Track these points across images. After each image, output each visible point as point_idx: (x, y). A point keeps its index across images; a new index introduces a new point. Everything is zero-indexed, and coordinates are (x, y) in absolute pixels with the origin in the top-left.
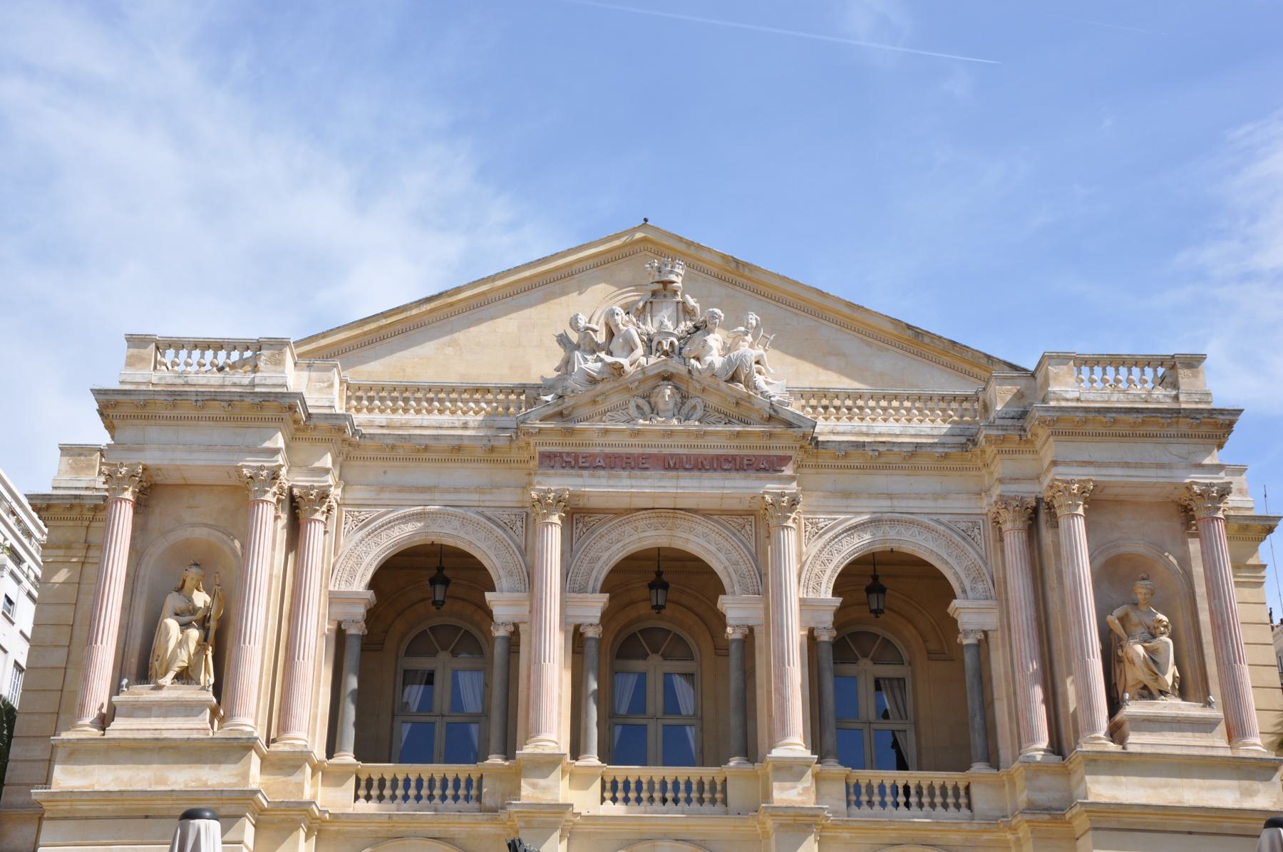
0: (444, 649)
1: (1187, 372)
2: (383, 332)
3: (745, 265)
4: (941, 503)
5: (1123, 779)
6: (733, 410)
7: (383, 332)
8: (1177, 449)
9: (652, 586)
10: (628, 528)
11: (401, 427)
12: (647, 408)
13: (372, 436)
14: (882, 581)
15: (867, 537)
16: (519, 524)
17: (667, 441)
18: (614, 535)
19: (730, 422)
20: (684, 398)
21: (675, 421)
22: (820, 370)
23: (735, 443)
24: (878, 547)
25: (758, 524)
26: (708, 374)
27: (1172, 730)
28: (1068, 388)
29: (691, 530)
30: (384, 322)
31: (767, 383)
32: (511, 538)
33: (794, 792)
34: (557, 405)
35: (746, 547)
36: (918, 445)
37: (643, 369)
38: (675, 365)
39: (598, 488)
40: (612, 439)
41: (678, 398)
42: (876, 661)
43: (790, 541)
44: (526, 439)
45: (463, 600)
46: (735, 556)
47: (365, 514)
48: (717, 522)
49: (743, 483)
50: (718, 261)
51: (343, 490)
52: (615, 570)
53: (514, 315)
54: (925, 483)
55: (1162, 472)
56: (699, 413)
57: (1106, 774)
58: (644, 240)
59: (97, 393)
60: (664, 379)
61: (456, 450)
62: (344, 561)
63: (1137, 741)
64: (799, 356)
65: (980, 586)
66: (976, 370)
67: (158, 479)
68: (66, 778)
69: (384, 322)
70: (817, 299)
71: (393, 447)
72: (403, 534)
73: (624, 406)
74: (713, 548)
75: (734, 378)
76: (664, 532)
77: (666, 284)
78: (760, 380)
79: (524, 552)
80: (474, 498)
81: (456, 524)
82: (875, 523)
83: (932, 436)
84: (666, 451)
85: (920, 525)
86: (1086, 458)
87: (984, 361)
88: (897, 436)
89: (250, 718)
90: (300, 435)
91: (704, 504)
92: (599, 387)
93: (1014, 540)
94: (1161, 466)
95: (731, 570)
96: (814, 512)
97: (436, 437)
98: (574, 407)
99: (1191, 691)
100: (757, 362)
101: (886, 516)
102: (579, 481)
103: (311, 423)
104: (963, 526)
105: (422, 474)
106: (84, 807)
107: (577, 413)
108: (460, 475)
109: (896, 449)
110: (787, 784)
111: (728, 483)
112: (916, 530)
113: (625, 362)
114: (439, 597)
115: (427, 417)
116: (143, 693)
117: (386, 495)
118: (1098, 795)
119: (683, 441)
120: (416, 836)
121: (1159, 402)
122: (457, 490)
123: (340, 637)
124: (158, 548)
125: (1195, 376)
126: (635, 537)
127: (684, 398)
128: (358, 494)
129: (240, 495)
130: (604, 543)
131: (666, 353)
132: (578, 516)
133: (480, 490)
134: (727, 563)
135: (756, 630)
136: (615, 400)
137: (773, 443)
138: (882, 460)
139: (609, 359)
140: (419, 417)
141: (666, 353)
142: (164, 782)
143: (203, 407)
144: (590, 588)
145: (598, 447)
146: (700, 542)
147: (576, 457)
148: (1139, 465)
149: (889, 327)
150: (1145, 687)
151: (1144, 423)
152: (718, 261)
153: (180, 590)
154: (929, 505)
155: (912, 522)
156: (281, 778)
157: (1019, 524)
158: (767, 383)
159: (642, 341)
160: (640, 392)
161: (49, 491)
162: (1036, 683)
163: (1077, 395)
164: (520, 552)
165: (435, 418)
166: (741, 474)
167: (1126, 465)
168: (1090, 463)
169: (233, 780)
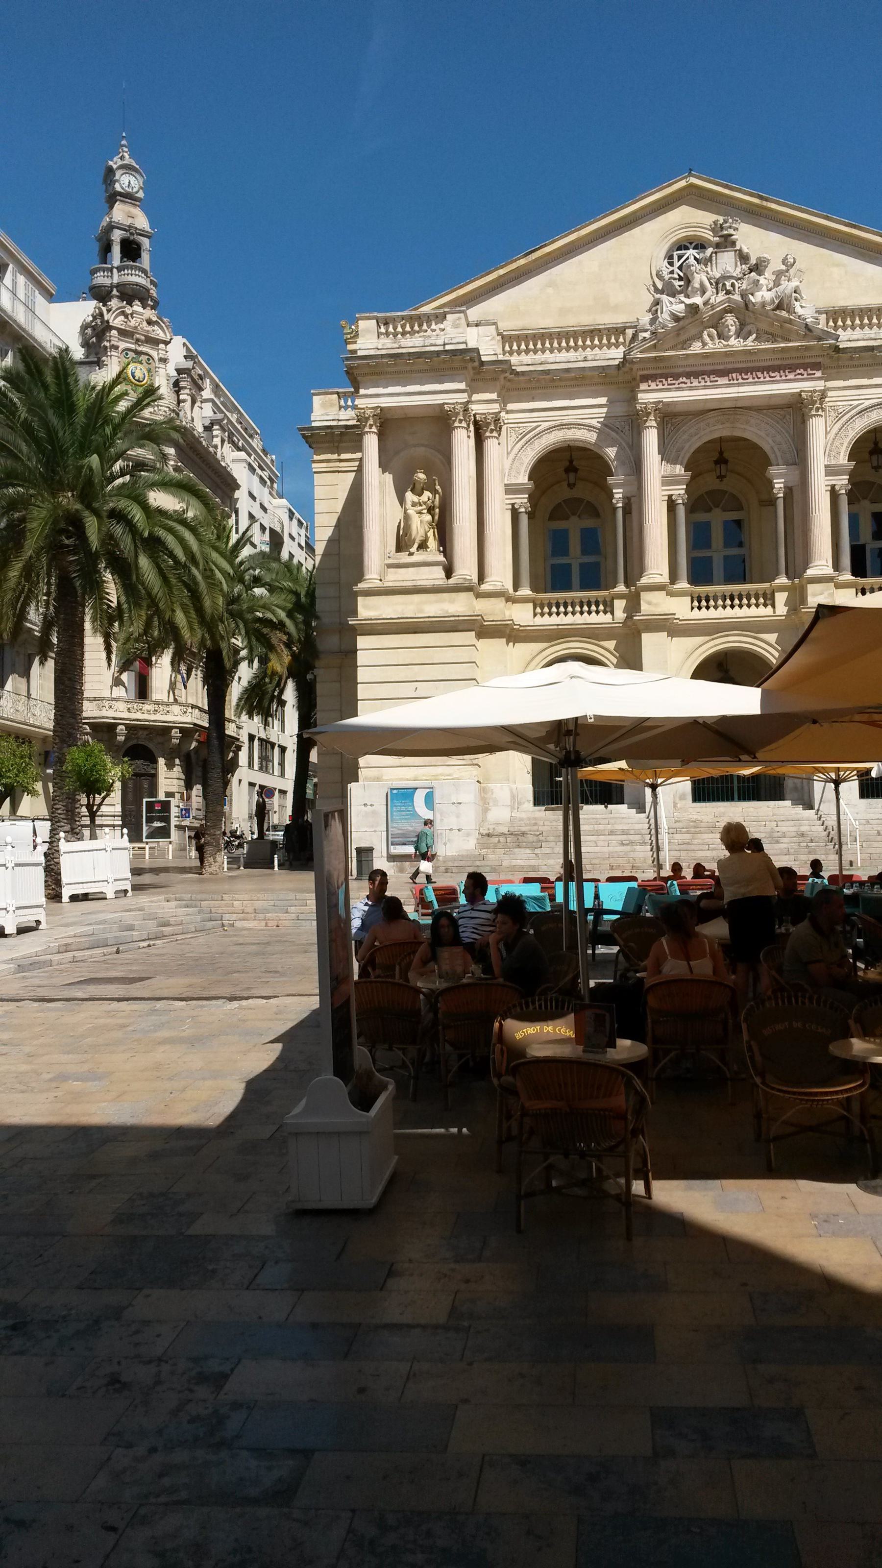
13: (523, 373)
14: (726, 455)
16: (627, 428)
18: (692, 430)
19: (776, 341)
25: (796, 413)
29: (747, 422)
31: (802, 307)
32: (622, 438)
35: (787, 432)
44: (630, 366)
45: (739, 474)
46: (779, 438)
48: (766, 415)
62: (510, 463)
67: (389, 416)
74: (762, 434)
75: (779, 307)
78: (798, 309)
79: (631, 447)
89: (466, 569)
92: (681, 323)
95: (776, 449)
97: (568, 370)
100: (795, 292)
114: (572, 481)
115: (558, 355)
116: (404, 557)
118: (540, 811)
130: (685, 437)
134: (773, 444)
135: (794, 489)
139: (688, 301)
140: (553, 355)
142: (421, 611)
146: (753, 431)
158: (802, 307)
159: (711, 284)
164: (629, 447)
165: (564, 356)
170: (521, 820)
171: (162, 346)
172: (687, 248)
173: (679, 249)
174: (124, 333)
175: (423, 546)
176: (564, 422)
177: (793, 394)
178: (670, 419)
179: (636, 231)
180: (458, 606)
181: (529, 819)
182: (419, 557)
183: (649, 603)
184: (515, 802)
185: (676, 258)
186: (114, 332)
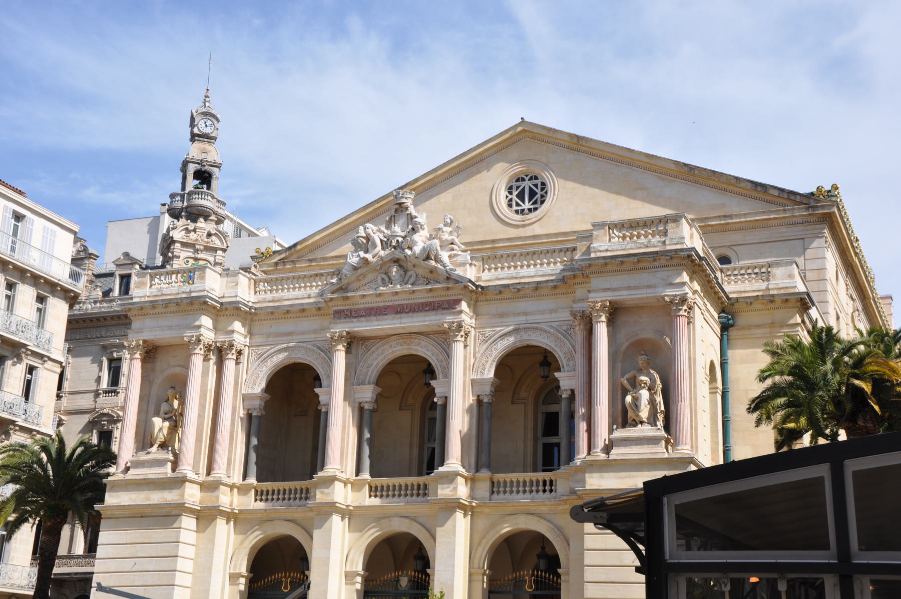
1: (673, 225)
2: (378, 212)
3: (583, 138)
4: (554, 315)
5: (606, 474)
6: (430, 276)
7: (378, 212)
8: (662, 274)
10: (387, 346)
11: (279, 301)
12: (387, 279)
13: (261, 308)
15: (512, 339)
17: (395, 298)
18: (380, 351)
20: (406, 271)
21: (398, 286)
22: (631, 201)
23: (430, 294)
24: (519, 345)
25: (444, 338)
26: (412, 258)
27: (637, 444)
28: (606, 245)
29: (419, 344)
30: (377, 206)
33: (448, 490)
34: (337, 284)
36: (538, 282)
37: (382, 258)
38: (398, 254)
39: (362, 327)
40: (367, 299)
41: (402, 273)
43: (458, 349)
47: (261, 350)
49: (434, 318)
50: (566, 138)
51: (250, 339)
53: (450, 191)
54: (547, 304)
55: (650, 291)
56: (411, 281)
57: (597, 472)
58: (524, 131)
60: (395, 262)
61: (303, 310)
62: (248, 379)
64: (618, 193)
66: (731, 188)
67: (157, 344)
68: (111, 499)
69: (377, 206)
70: (627, 154)
71: (272, 313)
72: (279, 359)
73: (375, 280)
75: (428, 258)
76: (405, 347)
77: (400, 204)
80: (312, 337)
81: (303, 351)
82: (516, 331)
83: (552, 275)
84: (396, 303)
85: (541, 329)
86: (609, 287)
87: (734, 181)
88: (533, 277)
90: (220, 313)
91: (423, 330)
92: (359, 271)
94: (649, 287)
96: (484, 328)
97: (291, 306)
98: (349, 284)
101: (522, 326)
102: (352, 325)
103: (224, 307)
104: (565, 328)
105: (288, 326)
106: (117, 513)
107: (351, 287)
108: (307, 324)
109: (526, 286)
110: (446, 486)
111: (426, 318)
112: (538, 333)
113: (369, 256)
116: (142, 456)
117: (271, 339)
119: (404, 296)
120: (279, 519)
121: (655, 246)
122: (304, 333)
123: (250, 416)
124: (159, 379)
125: (678, 227)
126: (391, 351)
127: (406, 271)
128: (258, 340)
129: (186, 349)
130: (374, 356)
131: (395, 247)
132: (353, 342)
133: (315, 332)
136: (370, 277)
137: (450, 292)
138: (521, 293)
141: (395, 247)
142: (149, 499)
143: (166, 307)
144: (367, 382)
145: (362, 305)
146: (424, 350)
148: (636, 288)
149: (672, 167)
151: (639, 261)
152: (566, 138)
153: (167, 401)
154: (547, 317)
155: (536, 328)
156: (209, 494)
157: (582, 327)
160: (383, 271)
162: (583, 420)
163: (606, 247)
166: (435, 312)
167: (629, 288)
168: (609, 289)
169: (177, 498)
171: (220, 252)
172: (523, 180)
173: (518, 180)
174: (184, 245)
176: (788, 285)
185: (514, 188)
186: (178, 245)
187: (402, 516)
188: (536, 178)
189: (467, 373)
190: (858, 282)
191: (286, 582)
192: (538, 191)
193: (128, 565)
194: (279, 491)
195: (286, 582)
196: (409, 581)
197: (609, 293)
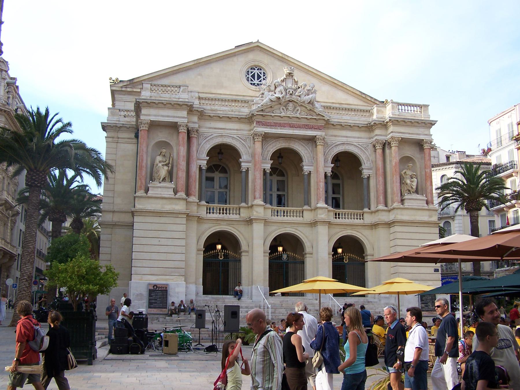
0: (217, 171)
9: (219, 153)
14: (223, 151)
42: (278, 175)
52: (274, 154)
55: (418, 136)
59: (102, 123)
63: (407, 204)
65: (369, 162)
93: (379, 151)
99: (419, 193)
104: (365, 146)
147: (266, 123)
150: (409, 191)
161: (106, 121)
170: (200, 300)
171: (4, 72)
172: (254, 69)
173: (251, 69)
175: (164, 180)
177: (313, 136)
178: (266, 138)
179: (235, 59)
180: (180, 207)
181: (203, 300)
182: (163, 184)
183: (257, 212)
184: (197, 294)
187: (217, 221)
188: (248, 72)
189: (317, 166)
190: (163, 126)
191: (221, 255)
192: (262, 76)
193: (163, 242)
194: (342, 213)
195: (221, 255)
196: (288, 256)
197: (401, 135)
